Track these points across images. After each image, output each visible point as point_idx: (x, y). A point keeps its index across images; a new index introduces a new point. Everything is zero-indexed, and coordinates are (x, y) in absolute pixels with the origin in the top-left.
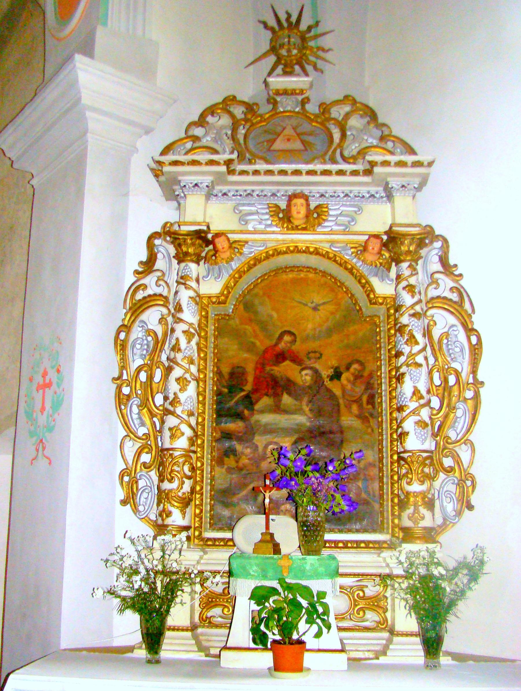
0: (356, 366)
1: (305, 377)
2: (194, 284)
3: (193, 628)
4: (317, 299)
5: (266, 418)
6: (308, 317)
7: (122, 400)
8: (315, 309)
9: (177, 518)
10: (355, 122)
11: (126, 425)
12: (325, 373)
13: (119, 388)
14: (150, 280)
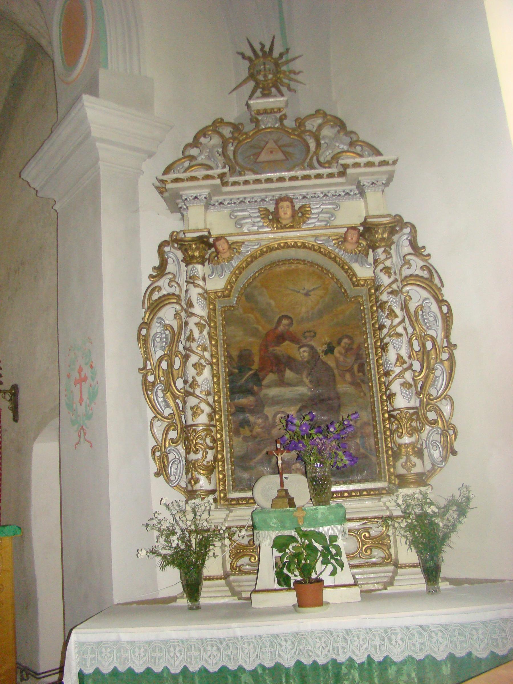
0: (346, 341)
1: (304, 354)
2: (201, 283)
3: (226, 576)
4: (308, 286)
5: (273, 392)
6: (302, 301)
7: (148, 387)
8: (307, 294)
9: (203, 484)
10: (327, 132)
11: (153, 407)
12: (320, 349)
13: (145, 377)
14: (163, 282)
